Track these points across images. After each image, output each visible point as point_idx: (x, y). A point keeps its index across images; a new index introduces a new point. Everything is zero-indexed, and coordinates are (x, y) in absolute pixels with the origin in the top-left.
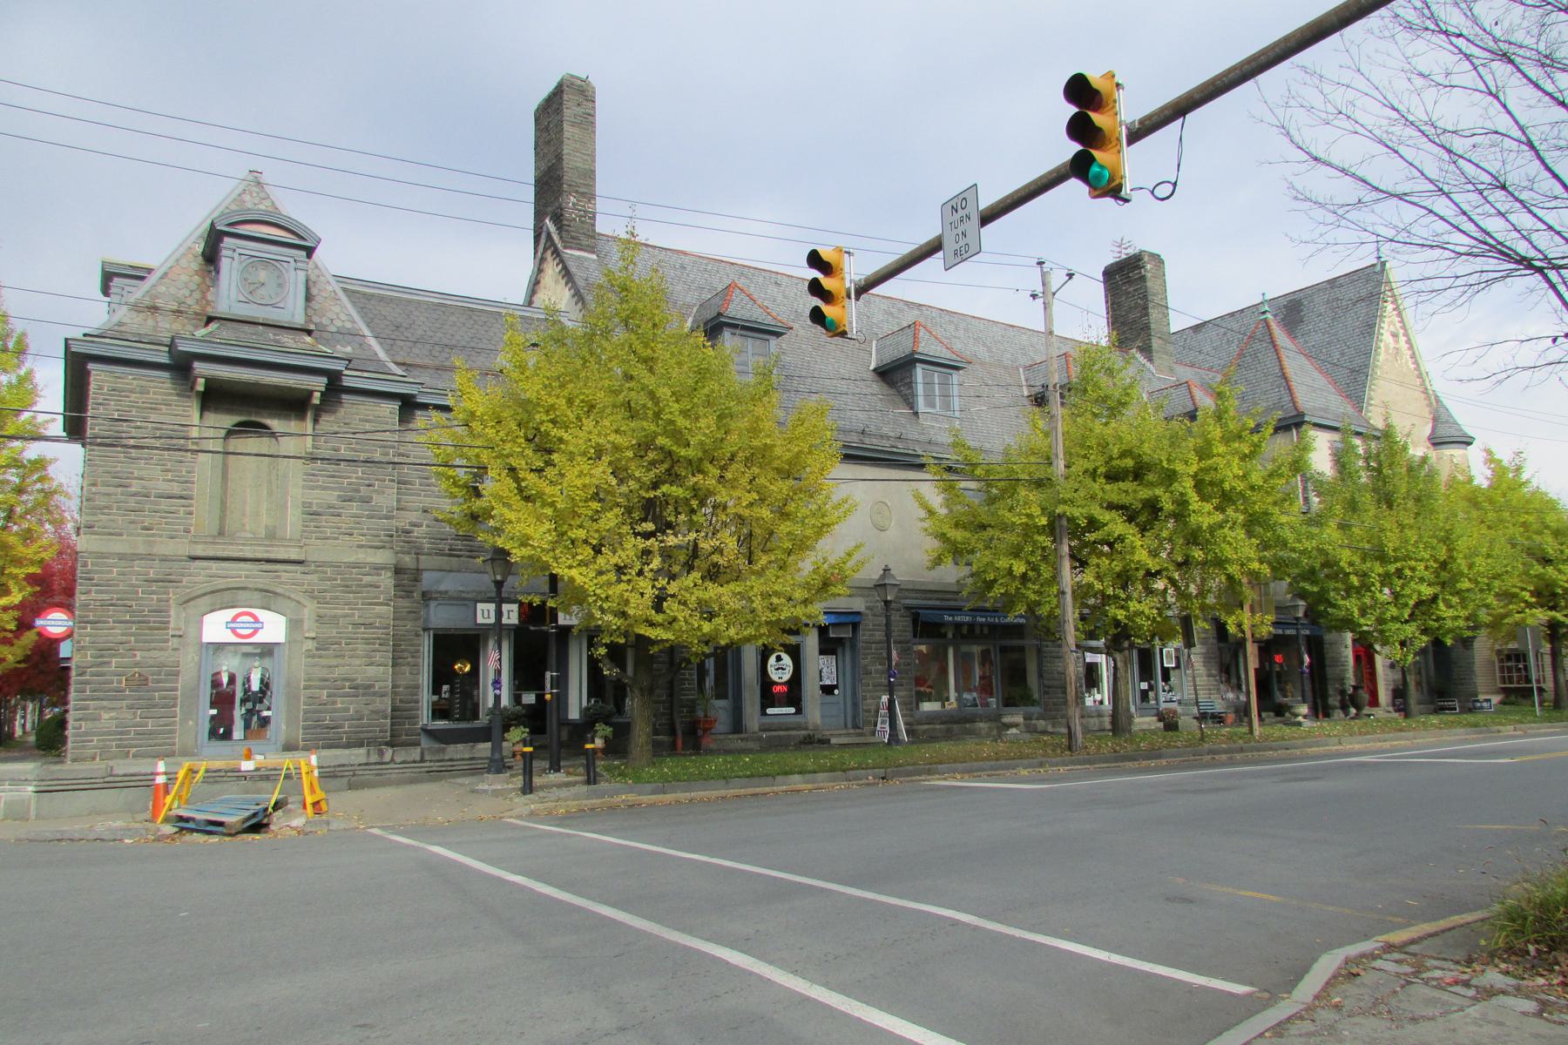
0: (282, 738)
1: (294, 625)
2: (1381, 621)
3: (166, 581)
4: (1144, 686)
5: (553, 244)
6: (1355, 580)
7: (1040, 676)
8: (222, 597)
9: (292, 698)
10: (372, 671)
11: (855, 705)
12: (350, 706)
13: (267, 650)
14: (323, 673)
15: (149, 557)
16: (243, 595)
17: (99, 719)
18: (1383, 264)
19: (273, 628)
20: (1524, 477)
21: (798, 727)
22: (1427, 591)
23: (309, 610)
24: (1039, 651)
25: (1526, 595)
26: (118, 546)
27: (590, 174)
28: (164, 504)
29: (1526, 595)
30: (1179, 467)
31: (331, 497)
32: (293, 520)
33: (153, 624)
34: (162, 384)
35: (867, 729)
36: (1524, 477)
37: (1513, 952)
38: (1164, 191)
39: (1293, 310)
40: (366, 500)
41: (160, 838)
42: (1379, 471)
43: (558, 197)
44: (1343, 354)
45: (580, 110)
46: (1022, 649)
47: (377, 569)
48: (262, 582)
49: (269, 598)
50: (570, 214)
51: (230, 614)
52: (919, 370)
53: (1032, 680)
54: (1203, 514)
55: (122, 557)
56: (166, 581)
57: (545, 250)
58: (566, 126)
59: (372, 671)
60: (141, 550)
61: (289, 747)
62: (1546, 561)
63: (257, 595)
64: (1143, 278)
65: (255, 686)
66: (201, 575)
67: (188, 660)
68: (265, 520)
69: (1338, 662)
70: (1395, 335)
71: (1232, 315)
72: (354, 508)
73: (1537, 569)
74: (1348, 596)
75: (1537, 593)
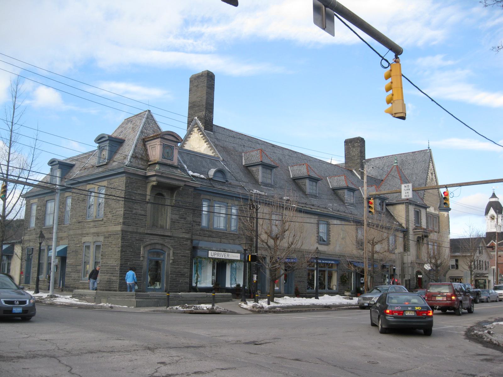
15: (137, 233)
31: (177, 217)
40: (185, 219)
48: (161, 242)
55: (131, 232)
60: (135, 231)
70: (432, 174)
72: (182, 221)
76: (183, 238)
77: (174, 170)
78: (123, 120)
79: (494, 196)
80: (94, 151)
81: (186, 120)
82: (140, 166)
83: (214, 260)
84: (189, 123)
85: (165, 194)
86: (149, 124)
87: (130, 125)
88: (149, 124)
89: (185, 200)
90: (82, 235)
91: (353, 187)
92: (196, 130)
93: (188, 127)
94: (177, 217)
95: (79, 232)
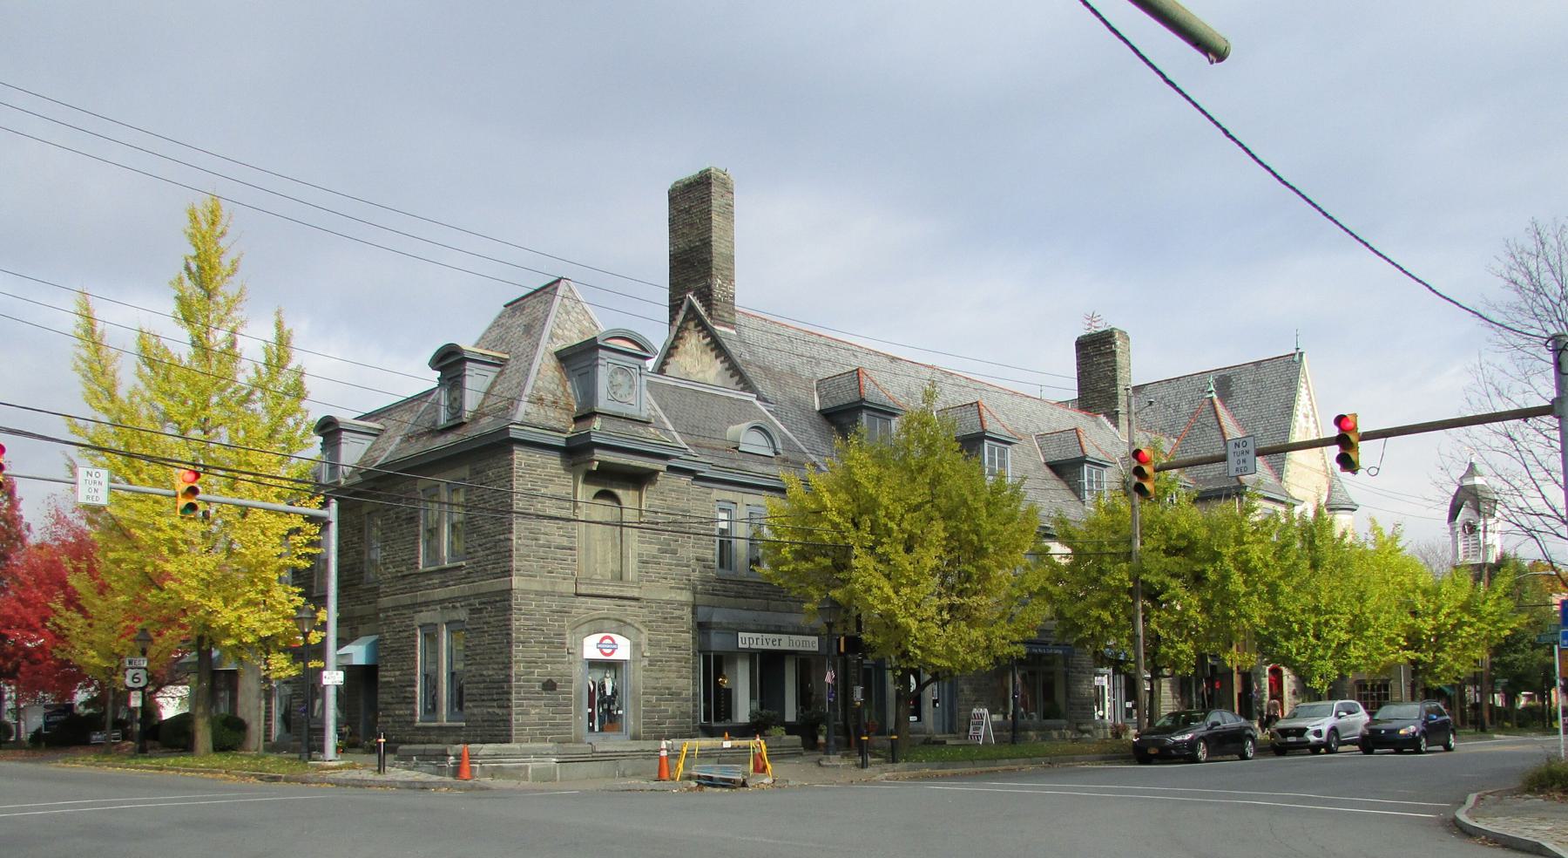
0: (631, 731)
1: (635, 647)
2: (1311, 658)
3: (563, 612)
4: (1129, 705)
5: (697, 316)
6: (1296, 627)
7: (1067, 695)
8: (596, 625)
9: (636, 701)
10: (682, 682)
11: (952, 715)
12: (670, 708)
13: (613, 666)
14: (653, 683)
15: (552, 594)
16: (607, 624)
17: (528, 714)
18: (1301, 354)
19: (623, 650)
20: (1400, 545)
21: (920, 732)
22: (1344, 637)
23: (645, 637)
24: (1067, 676)
25: (1401, 640)
26: (536, 586)
27: (730, 259)
28: (560, 554)
29: (1401, 640)
30: (1224, 551)
31: (653, 549)
32: (632, 567)
33: (557, 645)
34: (554, 462)
35: (962, 734)
36: (1400, 545)
37: (1529, 791)
38: (1373, 471)
39: (1225, 382)
40: (674, 552)
41: (691, 789)
42: (1312, 542)
43: (694, 268)
44: (1266, 430)
45: (723, 201)
46: (1052, 673)
47: (682, 605)
48: (616, 614)
49: (622, 626)
50: (717, 294)
51: (597, 637)
52: (986, 443)
53: (1060, 696)
54: (1237, 583)
55: (537, 593)
56: (563, 612)
57: (685, 319)
58: (714, 216)
59: (682, 682)
60: (549, 588)
61: (635, 737)
62: (1414, 614)
63: (614, 624)
64: (1114, 353)
65: (609, 692)
66: (583, 606)
67: (578, 671)
68: (610, 566)
69: (1260, 691)
70: (1306, 416)
71: (1169, 381)
72: (667, 558)
73: (1411, 620)
74: (1288, 638)
75: (1407, 639)
76: (669, 602)
77: (641, 430)
78: (879, 772)
79: (1472, 470)
80: (431, 392)
81: (664, 296)
82: (553, 423)
83: (751, 654)
84: (674, 309)
85: (619, 492)
86: (568, 313)
87: (520, 320)
88: (568, 313)
89: (249, 464)
90: (416, 607)
91: (1101, 456)
92: (691, 325)
93: (672, 319)
94: (653, 549)
95: (406, 599)
